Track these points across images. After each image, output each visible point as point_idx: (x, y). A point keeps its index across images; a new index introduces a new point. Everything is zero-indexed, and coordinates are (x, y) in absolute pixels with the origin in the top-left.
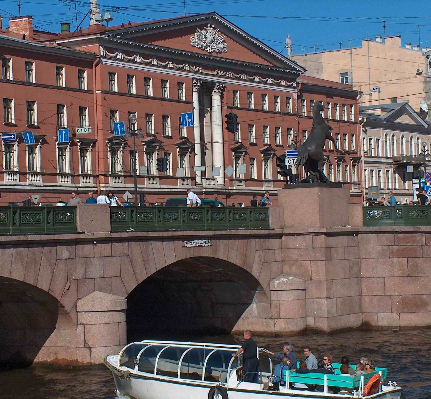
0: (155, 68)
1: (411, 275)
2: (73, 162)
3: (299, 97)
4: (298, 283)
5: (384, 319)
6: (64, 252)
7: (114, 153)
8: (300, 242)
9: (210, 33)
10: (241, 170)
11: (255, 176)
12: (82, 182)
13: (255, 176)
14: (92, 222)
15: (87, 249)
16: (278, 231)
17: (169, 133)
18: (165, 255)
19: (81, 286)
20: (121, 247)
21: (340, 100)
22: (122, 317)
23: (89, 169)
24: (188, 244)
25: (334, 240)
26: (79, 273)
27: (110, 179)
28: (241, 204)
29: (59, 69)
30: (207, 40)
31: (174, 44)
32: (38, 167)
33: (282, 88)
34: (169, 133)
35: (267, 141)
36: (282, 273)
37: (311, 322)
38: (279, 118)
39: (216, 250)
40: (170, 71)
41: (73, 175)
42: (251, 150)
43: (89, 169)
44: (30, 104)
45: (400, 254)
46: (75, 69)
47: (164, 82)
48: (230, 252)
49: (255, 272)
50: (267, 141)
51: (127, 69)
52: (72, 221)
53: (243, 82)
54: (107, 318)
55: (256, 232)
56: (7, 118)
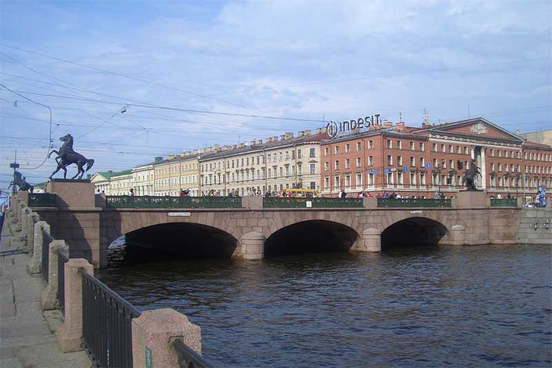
0: (453, 141)
1: (507, 226)
2: (417, 180)
3: (523, 151)
4: (463, 228)
5: (497, 241)
6: (358, 214)
7: (435, 176)
8: (463, 212)
9: (479, 126)
10: (493, 183)
11: (501, 185)
12: (421, 188)
13: (501, 185)
14: (370, 203)
15: (367, 213)
16: (247, 208)
17: (513, 171)
18: (400, 216)
19: (363, 225)
20: (383, 212)
21: (544, 153)
22: (379, 237)
23: (392, 182)
24: (412, 212)
25: (475, 212)
26: (364, 221)
27: (433, 187)
28: (423, 197)
29: (411, 143)
30: (479, 129)
31: (462, 131)
32: (402, 182)
33: (514, 148)
34: (513, 171)
35: (507, 170)
36: (457, 224)
37: (466, 242)
38: (508, 160)
39: (425, 215)
40: (461, 142)
41: (417, 185)
42: (499, 175)
43: (424, 182)
44: (399, 157)
45: (503, 217)
46: (419, 142)
47: (450, 146)
48: (433, 216)
49: (444, 223)
50: (507, 170)
51: (456, 144)
52: (362, 203)
53: (495, 146)
54: (254, 242)
55: (226, 209)
56: (411, 164)
